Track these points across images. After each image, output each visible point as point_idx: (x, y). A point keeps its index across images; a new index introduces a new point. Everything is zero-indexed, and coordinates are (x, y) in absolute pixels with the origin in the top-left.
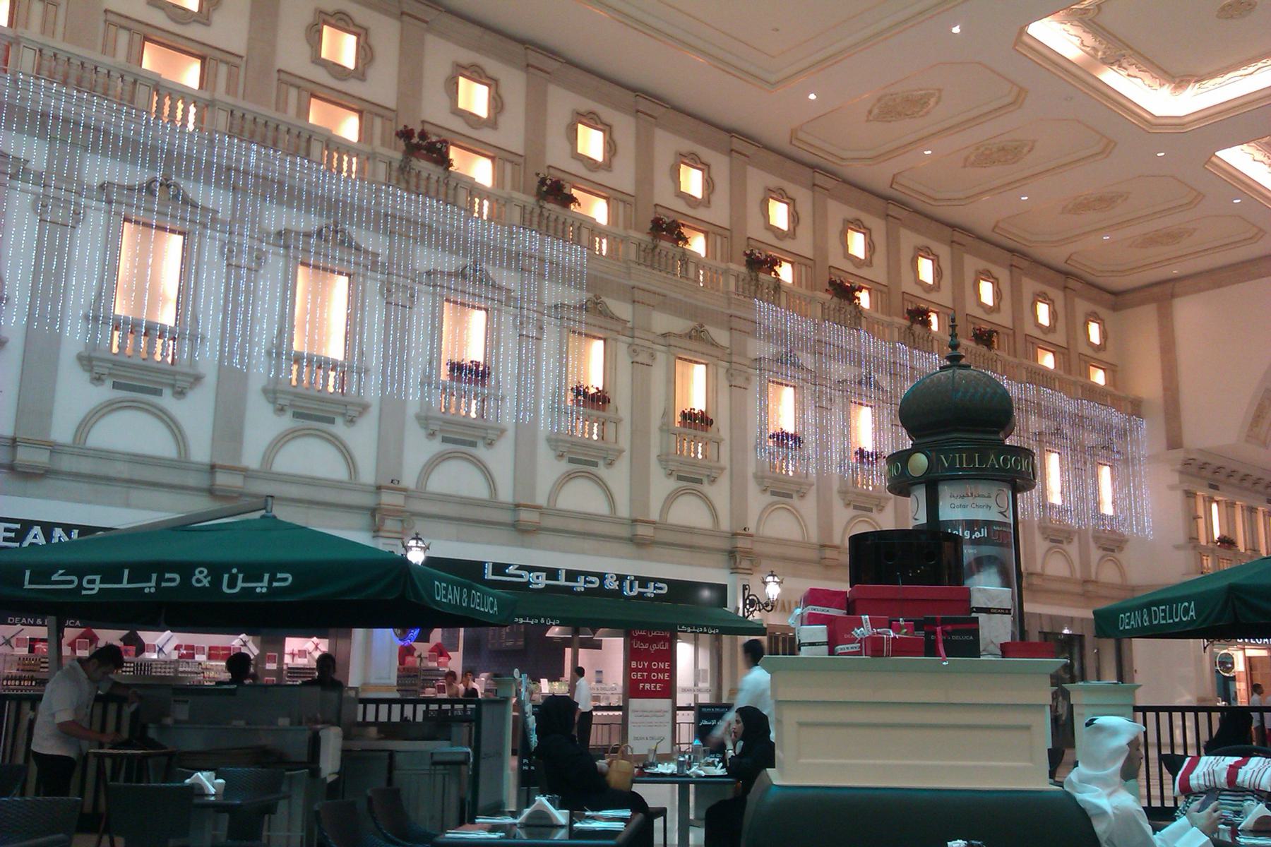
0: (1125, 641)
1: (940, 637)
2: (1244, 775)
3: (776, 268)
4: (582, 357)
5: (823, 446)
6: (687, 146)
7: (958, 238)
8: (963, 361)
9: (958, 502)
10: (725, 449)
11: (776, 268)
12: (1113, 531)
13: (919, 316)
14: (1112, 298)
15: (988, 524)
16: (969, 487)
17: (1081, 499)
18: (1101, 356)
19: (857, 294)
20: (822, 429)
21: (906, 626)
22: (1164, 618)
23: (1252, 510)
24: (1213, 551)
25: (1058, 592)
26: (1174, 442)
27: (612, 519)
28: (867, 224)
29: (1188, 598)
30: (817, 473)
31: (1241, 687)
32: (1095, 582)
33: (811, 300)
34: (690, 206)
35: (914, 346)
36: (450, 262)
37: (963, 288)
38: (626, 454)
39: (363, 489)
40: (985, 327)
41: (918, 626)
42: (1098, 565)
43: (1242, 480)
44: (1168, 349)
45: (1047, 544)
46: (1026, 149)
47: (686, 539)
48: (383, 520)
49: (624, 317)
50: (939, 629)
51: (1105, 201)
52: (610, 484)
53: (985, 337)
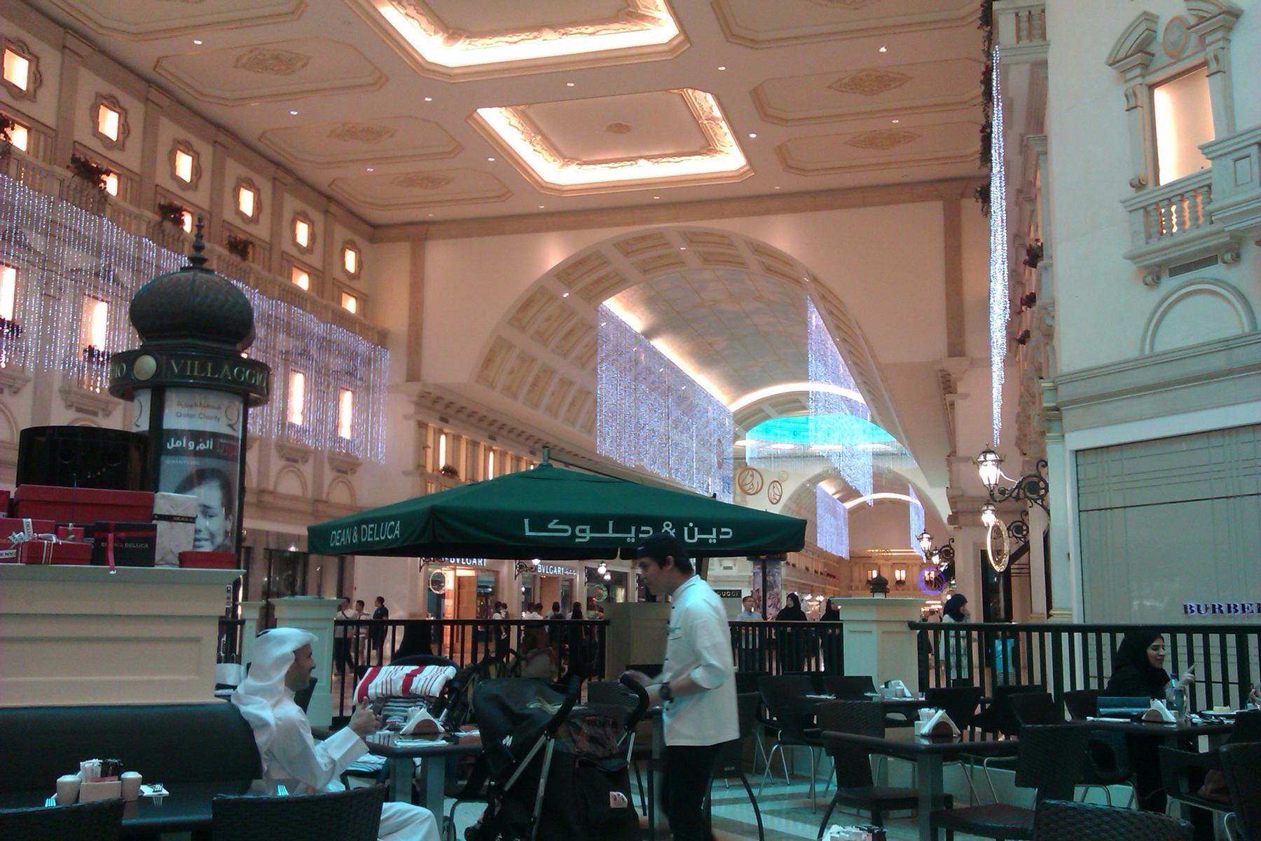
0: (349, 558)
1: (111, 545)
2: (418, 684)
3: (8, 130)
5: (47, 338)
6: (107, 88)
7: (222, 139)
8: (206, 266)
9: (185, 411)
11: (8, 130)
12: (347, 454)
13: (171, 213)
14: (370, 230)
15: (215, 436)
16: (198, 397)
17: (320, 421)
18: (307, 259)
19: (104, 177)
20: (47, 320)
21: (74, 532)
22: (372, 536)
23: (475, 444)
24: (437, 478)
25: (290, 511)
26: (413, 375)
29: (395, 518)
30: (36, 365)
31: (449, 604)
32: (325, 502)
33: (50, 174)
35: (162, 244)
37: (223, 195)
40: (241, 236)
41: (88, 533)
42: (330, 485)
43: (458, 412)
45: (334, 474)
46: (300, 64)
50: (111, 536)
51: (374, 134)
53: (240, 247)
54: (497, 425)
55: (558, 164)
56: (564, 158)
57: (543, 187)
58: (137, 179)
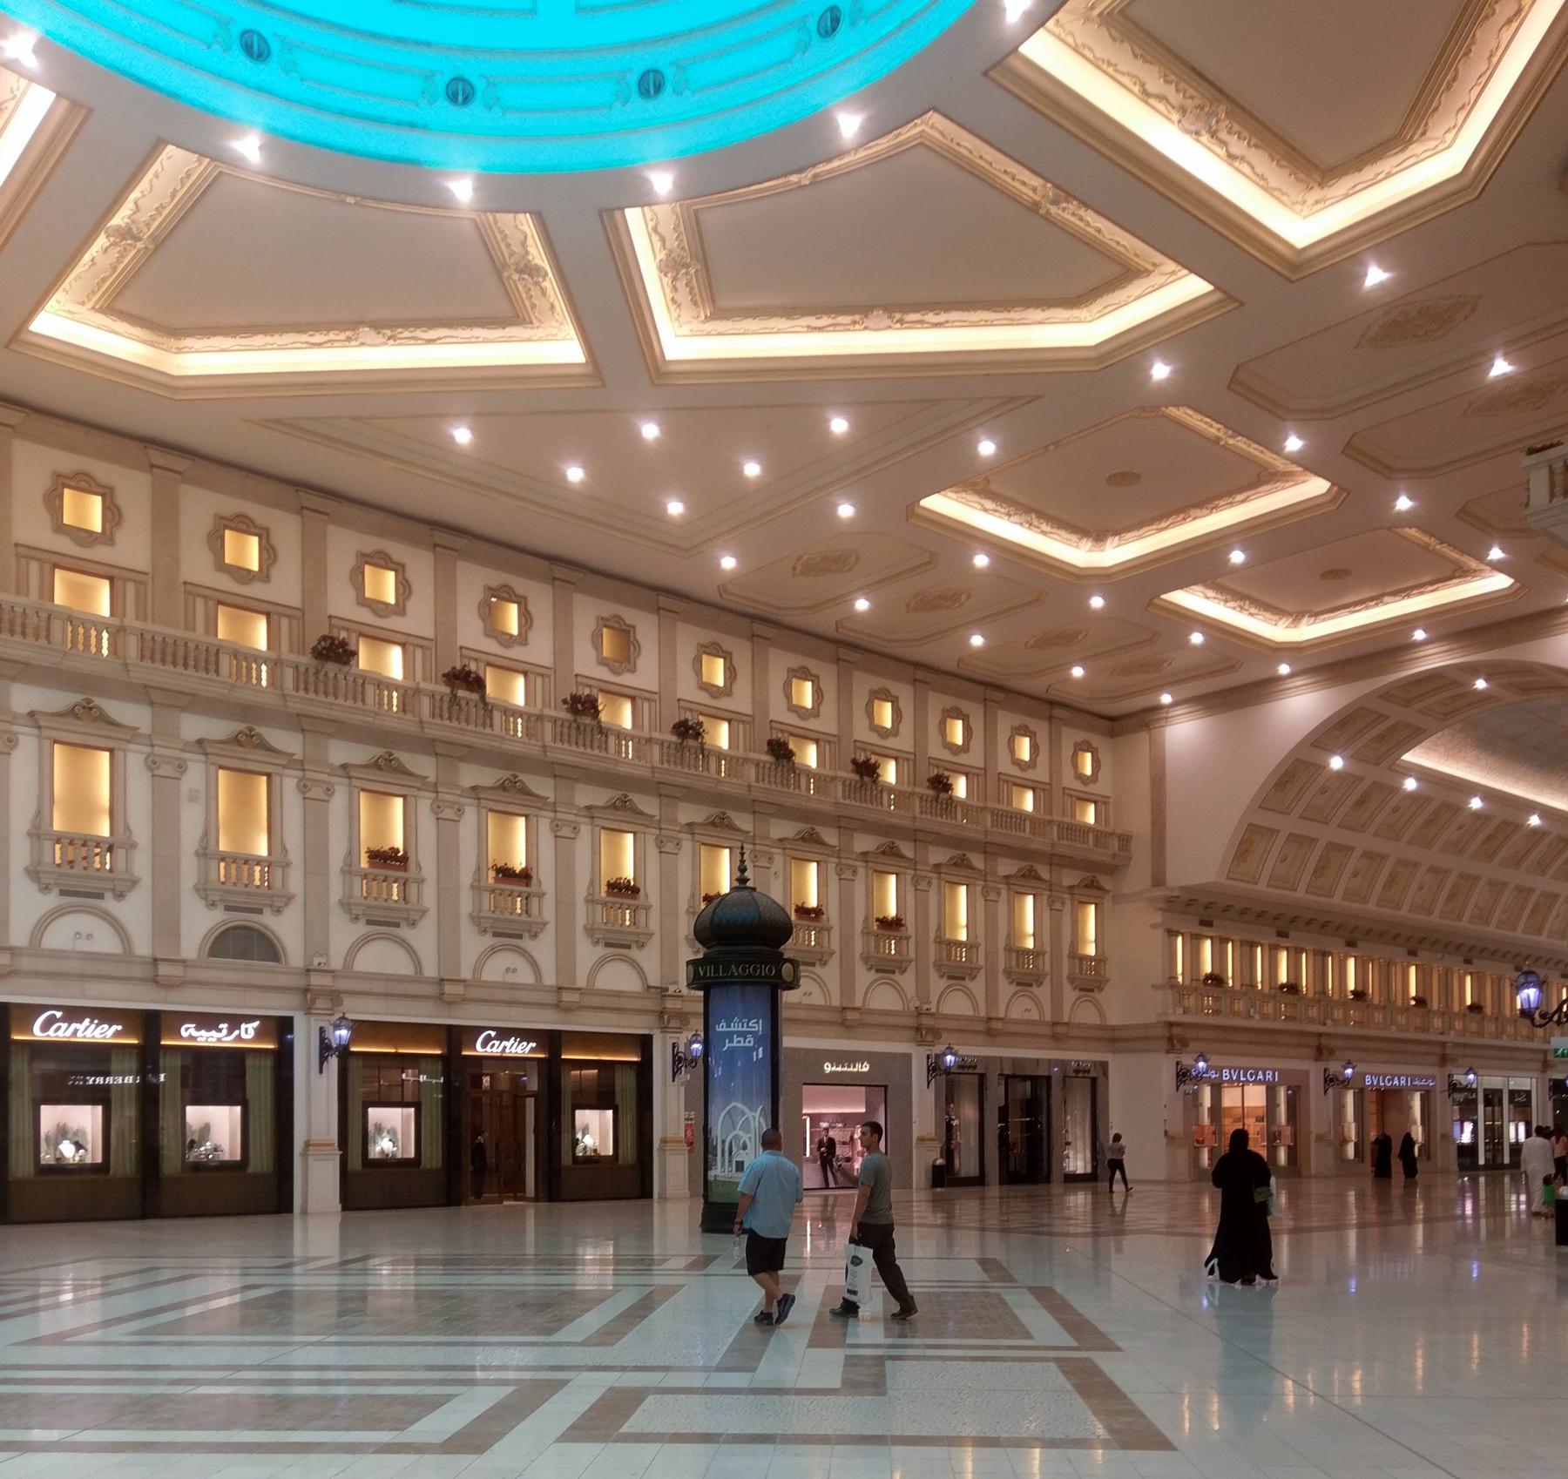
4: (714, 864)
10: (835, 934)
26: (1158, 880)
27: (418, 977)
28: (894, 692)
34: (714, 697)
36: (59, 700)
38: (656, 940)
39: (429, 981)
45: (1076, 994)
47: (614, 1002)
48: (313, 1001)
49: (290, 751)
52: (414, 944)
58: (432, 645)
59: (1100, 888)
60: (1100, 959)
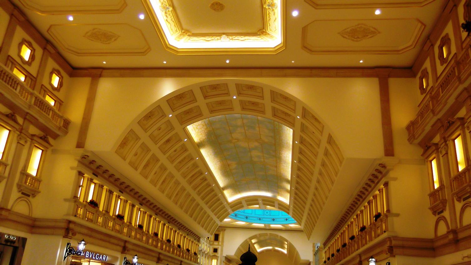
23: (133, 206)
24: (85, 206)
26: (80, 145)
43: (104, 172)
44: (91, 100)
54: (124, 186)
55: (179, 32)
56: (182, 29)
57: (167, 47)
59: (48, 142)
60: (37, 180)
